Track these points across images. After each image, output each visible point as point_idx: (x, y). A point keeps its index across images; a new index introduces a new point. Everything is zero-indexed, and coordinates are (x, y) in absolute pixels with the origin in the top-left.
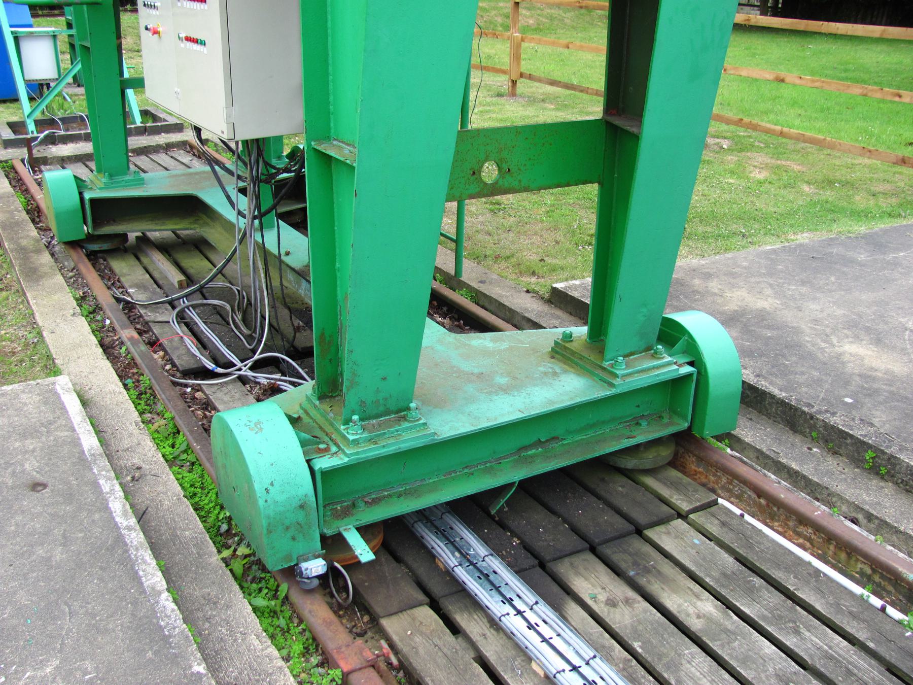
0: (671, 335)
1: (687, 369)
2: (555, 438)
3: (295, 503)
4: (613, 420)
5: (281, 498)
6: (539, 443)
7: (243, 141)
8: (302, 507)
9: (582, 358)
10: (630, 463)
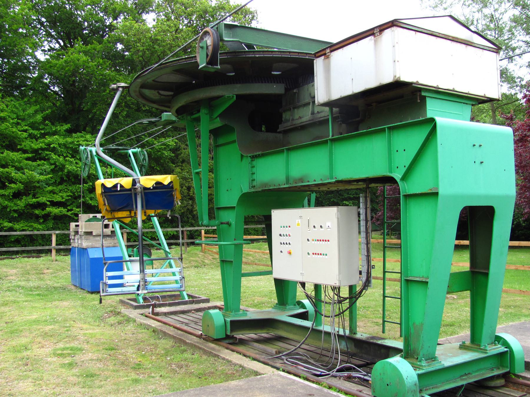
0: (498, 339)
1: (506, 349)
2: (469, 373)
3: (414, 383)
4: (484, 368)
5: (410, 381)
6: (466, 375)
7: (511, 239)
8: (415, 385)
9: (472, 347)
10: (493, 384)
